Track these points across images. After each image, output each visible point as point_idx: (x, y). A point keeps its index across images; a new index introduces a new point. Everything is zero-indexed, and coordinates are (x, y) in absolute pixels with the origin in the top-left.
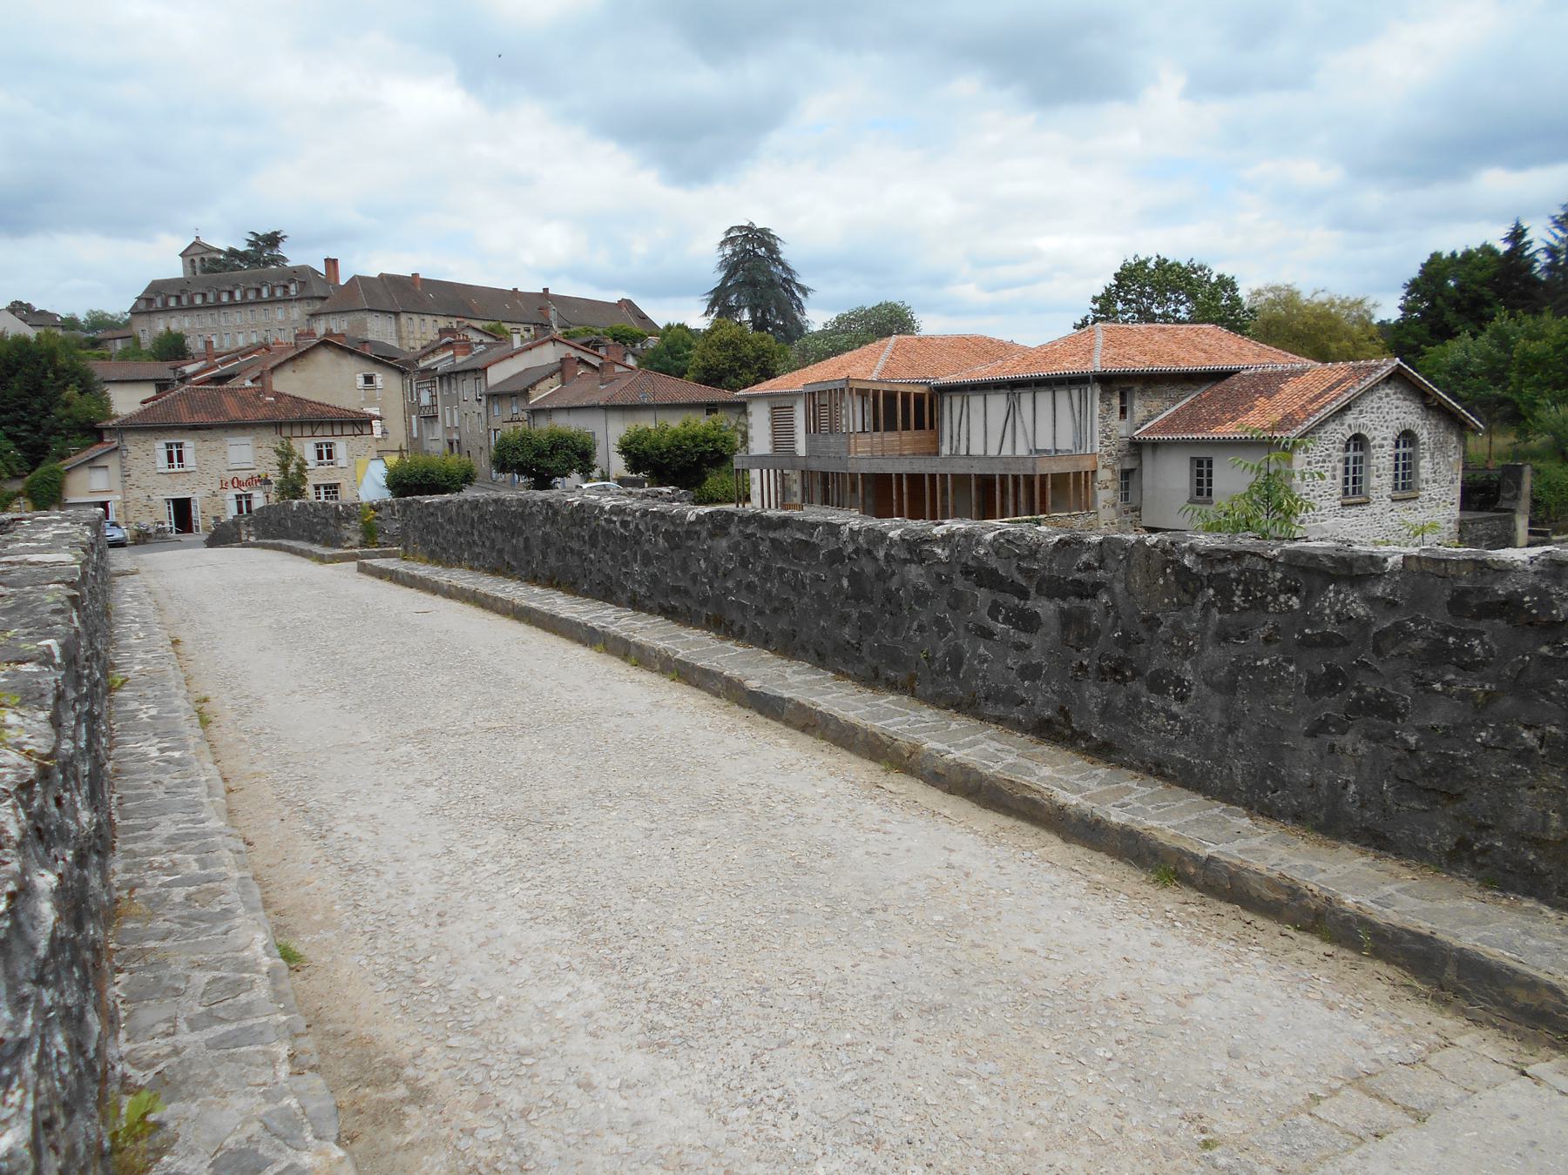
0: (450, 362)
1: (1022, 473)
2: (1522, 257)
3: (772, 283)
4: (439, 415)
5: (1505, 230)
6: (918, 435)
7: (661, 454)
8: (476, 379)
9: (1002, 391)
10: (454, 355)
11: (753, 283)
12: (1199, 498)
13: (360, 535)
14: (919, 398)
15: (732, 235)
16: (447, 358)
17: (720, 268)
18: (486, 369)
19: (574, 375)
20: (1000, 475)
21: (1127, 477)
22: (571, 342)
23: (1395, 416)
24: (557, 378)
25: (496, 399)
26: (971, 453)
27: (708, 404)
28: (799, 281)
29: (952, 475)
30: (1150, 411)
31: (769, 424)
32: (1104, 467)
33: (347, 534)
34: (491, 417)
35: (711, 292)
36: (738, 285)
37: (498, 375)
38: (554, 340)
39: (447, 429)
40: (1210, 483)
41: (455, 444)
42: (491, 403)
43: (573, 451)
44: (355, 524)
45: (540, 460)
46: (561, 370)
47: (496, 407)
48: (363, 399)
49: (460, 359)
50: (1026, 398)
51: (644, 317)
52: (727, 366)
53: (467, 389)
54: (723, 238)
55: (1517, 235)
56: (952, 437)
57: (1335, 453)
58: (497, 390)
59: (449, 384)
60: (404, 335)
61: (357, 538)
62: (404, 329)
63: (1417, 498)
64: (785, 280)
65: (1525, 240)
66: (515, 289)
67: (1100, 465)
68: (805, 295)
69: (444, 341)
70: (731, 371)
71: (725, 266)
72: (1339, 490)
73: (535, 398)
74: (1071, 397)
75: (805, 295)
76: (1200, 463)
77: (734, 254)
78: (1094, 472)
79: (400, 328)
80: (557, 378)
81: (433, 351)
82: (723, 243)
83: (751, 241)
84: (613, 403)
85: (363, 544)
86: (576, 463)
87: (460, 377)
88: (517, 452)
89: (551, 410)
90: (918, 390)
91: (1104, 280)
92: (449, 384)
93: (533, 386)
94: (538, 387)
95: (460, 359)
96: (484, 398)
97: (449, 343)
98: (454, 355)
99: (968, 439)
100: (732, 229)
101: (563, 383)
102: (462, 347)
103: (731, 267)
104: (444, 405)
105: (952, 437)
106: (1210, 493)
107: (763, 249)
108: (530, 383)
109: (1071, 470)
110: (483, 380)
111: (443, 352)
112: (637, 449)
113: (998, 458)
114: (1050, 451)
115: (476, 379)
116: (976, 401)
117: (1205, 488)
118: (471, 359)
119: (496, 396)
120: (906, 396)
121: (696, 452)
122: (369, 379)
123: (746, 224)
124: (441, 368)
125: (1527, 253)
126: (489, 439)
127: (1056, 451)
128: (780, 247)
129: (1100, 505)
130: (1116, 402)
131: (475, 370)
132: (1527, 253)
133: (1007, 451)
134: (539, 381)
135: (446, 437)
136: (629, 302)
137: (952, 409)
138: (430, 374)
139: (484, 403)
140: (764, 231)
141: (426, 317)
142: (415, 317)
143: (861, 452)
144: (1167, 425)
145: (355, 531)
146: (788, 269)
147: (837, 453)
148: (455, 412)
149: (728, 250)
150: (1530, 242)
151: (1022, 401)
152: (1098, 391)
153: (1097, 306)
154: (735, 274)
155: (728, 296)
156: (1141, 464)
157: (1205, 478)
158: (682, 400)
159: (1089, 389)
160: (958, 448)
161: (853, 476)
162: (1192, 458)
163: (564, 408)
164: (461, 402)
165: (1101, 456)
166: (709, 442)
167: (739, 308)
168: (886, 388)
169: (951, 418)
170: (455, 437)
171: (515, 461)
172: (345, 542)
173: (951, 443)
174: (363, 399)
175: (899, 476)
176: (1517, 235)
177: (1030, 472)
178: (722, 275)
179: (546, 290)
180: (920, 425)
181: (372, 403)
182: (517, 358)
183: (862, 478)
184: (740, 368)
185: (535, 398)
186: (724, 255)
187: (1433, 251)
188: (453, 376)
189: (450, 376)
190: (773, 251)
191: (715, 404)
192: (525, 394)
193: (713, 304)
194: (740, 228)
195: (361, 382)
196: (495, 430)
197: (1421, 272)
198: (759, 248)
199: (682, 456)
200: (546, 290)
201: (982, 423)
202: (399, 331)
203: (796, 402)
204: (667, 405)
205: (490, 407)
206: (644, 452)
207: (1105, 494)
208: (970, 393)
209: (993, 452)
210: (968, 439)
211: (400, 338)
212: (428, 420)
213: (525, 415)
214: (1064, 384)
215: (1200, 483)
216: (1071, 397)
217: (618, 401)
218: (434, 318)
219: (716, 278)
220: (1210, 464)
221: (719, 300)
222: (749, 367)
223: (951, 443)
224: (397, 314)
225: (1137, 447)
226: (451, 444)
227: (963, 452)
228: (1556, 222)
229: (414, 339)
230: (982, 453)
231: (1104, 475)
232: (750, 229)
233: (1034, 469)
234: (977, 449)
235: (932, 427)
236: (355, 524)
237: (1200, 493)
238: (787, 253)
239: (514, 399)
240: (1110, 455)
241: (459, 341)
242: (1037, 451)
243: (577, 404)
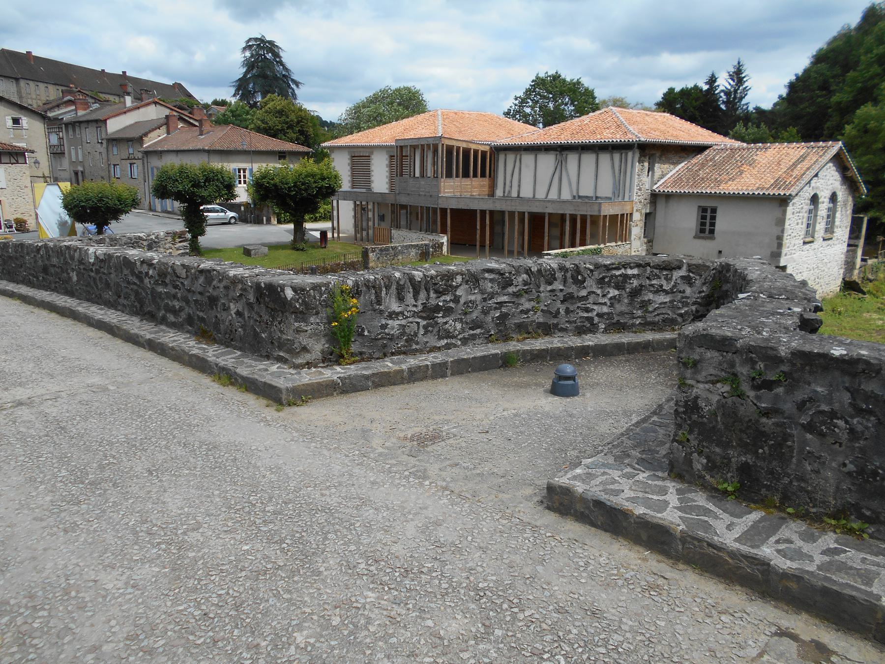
0: (72, 115)
1: (589, 213)
2: (714, 94)
3: (276, 78)
4: (66, 152)
5: (706, 79)
6: (482, 181)
7: (289, 188)
8: (97, 127)
9: (552, 152)
10: (76, 110)
11: (265, 77)
12: (702, 235)
13: (323, 341)
14: (484, 153)
15: (250, 44)
16: (69, 112)
17: (243, 66)
18: (106, 120)
19: (176, 128)
20: (570, 214)
21: (649, 217)
22: (167, 105)
23: (831, 182)
24: (164, 128)
25: (114, 143)
26: (521, 195)
27: (280, 152)
28: (294, 77)
29: (529, 213)
30: (663, 172)
31: (349, 168)
32: (637, 211)
33: (304, 340)
34: (111, 156)
35: (237, 81)
36: (254, 76)
37: (114, 125)
38: (156, 103)
39: (72, 163)
40: (713, 224)
41: (80, 174)
42: (110, 146)
43: (221, 183)
44: (315, 323)
45: (196, 190)
46: (166, 124)
47: (115, 150)
48: (12, 136)
49: (81, 113)
50: (572, 159)
51: (190, 96)
52: (279, 127)
53: (89, 135)
54: (244, 45)
55: (712, 80)
56: (505, 184)
57: (805, 207)
58: (116, 136)
59: (74, 131)
60: (24, 95)
61: (318, 347)
62: (23, 91)
63: (831, 239)
64: (284, 76)
65: (716, 84)
66: (103, 71)
67: (635, 209)
68: (298, 86)
69: (66, 99)
70: (282, 130)
71: (247, 65)
72: (803, 232)
73: (148, 143)
74: (612, 159)
75: (298, 86)
76: (704, 210)
77: (252, 56)
78: (631, 214)
79: (20, 89)
80: (164, 128)
81: (58, 106)
82: (244, 49)
83: (263, 48)
84: (214, 148)
85: (333, 358)
86: (223, 192)
87: (83, 126)
88: (177, 183)
89: (162, 152)
90: (482, 148)
91: (527, 83)
92: (74, 131)
93: (146, 134)
94: (149, 135)
95: (81, 113)
96: (104, 142)
97: (70, 101)
98: (76, 110)
99: (519, 186)
100: (250, 40)
101: (168, 133)
102: (81, 104)
103: (250, 65)
104: (70, 145)
105: (505, 184)
106: (712, 232)
107: (270, 54)
108: (143, 132)
109: (620, 213)
110: (103, 129)
111: (66, 107)
112: (268, 183)
113: (546, 201)
114: (592, 197)
115: (97, 127)
116: (528, 159)
117: (708, 227)
118: (89, 113)
119: (114, 141)
120: (476, 152)
121: (316, 187)
122: (16, 121)
123: (259, 37)
124: (67, 118)
125: (716, 92)
126: (109, 171)
127: (597, 198)
128: (281, 54)
129: (633, 237)
130: (646, 164)
131: (96, 121)
132: (716, 92)
133: (553, 195)
134: (150, 131)
135: (72, 168)
136: (180, 84)
137: (506, 165)
138: (58, 122)
139: (105, 145)
140: (271, 42)
141: (39, 84)
142: (31, 83)
143: (448, 192)
144: (678, 180)
145: (315, 335)
146: (287, 69)
147: (429, 192)
148: (80, 152)
149: (248, 54)
150: (718, 86)
151: (569, 160)
152: (637, 155)
153: (517, 102)
154: (252, 70)
155: (248, 84)
156: (655, 209)
157: (708, 221)
158: (262, 148)
159: (623, 155)
160: (510, 192)
161: (444, 211)
162: (699, 207)
163: (174, 151)
164: (84, 144)
165: (636, 203)
166: (325, 179)
167: (255, 92)
168: (465, 145)
169: (505, 170)
170: (80, 169)
171: (176, 190)
172: (297, 354)
173: (504, 188)
174: (12, 136)
175: (483, 212)
176: (712, 80)
177: (596, 213)
178: (244, 70)
179: (124, 73)
180: (483, 175)
181: (21, 139)
182: (128, 114)
183: (451, 212)
184: (288, 128)
185: (148, 143)
186: (245, 57)
187: (669, 87)
188: (78, 124)
189: (74, 125)
190: (276, 55)
191: (284, 152)
192: (140, 140)
193: (238, 90)
194: (256, 39)
195: (10, 123)
196: (114, 165)
197: (662, 98)
198: (268, 53)
199: (306, 190)
200: (124, 73)
201: (533, 174)
202: (19, 92)
203: (372, 153)
204: (218, 151)
205: (110, 149)
206: (275, 185)
207: (637, 231)
208: (523, 152)
209: (541, 195)
210: (519, 186)
211: (21, 97)
212: (57, 156)
213: (140, 155)
214: (607, 149)
215: (703, 224)
216: (612, 159)
217: (218, 148)
218: (46, 85)
219: (240, 72)
220: (714, 210)
221: (242, 86)
222: (292, 129)
223: (504, 188)
224: (17, 80)
225: (655, 197)
226: (76, 173)
227: (514, 194)
228: (730, 75)
229: (32, 99)
230: (531, 196)
231: (637, 216)
232: (262, 40)
233: (600, 211)
234: (526, 193)
235: (490, 176)
236: (315, 323)
237: (702, 231)
238: (286, 58)
239: (130, 143)
240: (640, 202)
241: (79, 99)
242: (580, 197)
243: (186, 148)
